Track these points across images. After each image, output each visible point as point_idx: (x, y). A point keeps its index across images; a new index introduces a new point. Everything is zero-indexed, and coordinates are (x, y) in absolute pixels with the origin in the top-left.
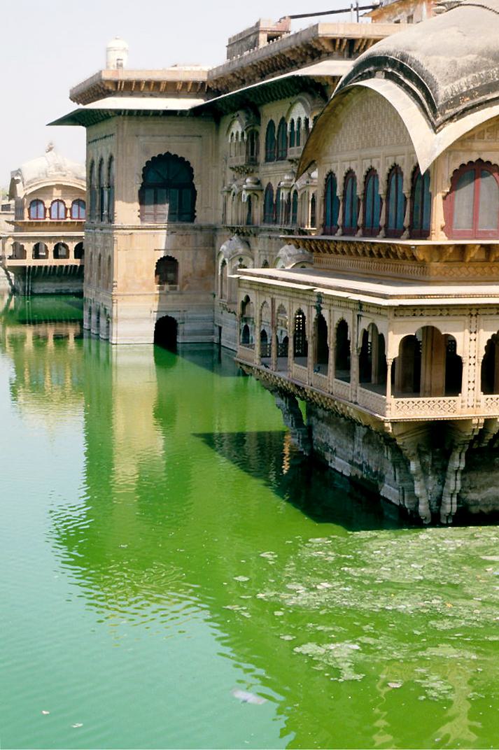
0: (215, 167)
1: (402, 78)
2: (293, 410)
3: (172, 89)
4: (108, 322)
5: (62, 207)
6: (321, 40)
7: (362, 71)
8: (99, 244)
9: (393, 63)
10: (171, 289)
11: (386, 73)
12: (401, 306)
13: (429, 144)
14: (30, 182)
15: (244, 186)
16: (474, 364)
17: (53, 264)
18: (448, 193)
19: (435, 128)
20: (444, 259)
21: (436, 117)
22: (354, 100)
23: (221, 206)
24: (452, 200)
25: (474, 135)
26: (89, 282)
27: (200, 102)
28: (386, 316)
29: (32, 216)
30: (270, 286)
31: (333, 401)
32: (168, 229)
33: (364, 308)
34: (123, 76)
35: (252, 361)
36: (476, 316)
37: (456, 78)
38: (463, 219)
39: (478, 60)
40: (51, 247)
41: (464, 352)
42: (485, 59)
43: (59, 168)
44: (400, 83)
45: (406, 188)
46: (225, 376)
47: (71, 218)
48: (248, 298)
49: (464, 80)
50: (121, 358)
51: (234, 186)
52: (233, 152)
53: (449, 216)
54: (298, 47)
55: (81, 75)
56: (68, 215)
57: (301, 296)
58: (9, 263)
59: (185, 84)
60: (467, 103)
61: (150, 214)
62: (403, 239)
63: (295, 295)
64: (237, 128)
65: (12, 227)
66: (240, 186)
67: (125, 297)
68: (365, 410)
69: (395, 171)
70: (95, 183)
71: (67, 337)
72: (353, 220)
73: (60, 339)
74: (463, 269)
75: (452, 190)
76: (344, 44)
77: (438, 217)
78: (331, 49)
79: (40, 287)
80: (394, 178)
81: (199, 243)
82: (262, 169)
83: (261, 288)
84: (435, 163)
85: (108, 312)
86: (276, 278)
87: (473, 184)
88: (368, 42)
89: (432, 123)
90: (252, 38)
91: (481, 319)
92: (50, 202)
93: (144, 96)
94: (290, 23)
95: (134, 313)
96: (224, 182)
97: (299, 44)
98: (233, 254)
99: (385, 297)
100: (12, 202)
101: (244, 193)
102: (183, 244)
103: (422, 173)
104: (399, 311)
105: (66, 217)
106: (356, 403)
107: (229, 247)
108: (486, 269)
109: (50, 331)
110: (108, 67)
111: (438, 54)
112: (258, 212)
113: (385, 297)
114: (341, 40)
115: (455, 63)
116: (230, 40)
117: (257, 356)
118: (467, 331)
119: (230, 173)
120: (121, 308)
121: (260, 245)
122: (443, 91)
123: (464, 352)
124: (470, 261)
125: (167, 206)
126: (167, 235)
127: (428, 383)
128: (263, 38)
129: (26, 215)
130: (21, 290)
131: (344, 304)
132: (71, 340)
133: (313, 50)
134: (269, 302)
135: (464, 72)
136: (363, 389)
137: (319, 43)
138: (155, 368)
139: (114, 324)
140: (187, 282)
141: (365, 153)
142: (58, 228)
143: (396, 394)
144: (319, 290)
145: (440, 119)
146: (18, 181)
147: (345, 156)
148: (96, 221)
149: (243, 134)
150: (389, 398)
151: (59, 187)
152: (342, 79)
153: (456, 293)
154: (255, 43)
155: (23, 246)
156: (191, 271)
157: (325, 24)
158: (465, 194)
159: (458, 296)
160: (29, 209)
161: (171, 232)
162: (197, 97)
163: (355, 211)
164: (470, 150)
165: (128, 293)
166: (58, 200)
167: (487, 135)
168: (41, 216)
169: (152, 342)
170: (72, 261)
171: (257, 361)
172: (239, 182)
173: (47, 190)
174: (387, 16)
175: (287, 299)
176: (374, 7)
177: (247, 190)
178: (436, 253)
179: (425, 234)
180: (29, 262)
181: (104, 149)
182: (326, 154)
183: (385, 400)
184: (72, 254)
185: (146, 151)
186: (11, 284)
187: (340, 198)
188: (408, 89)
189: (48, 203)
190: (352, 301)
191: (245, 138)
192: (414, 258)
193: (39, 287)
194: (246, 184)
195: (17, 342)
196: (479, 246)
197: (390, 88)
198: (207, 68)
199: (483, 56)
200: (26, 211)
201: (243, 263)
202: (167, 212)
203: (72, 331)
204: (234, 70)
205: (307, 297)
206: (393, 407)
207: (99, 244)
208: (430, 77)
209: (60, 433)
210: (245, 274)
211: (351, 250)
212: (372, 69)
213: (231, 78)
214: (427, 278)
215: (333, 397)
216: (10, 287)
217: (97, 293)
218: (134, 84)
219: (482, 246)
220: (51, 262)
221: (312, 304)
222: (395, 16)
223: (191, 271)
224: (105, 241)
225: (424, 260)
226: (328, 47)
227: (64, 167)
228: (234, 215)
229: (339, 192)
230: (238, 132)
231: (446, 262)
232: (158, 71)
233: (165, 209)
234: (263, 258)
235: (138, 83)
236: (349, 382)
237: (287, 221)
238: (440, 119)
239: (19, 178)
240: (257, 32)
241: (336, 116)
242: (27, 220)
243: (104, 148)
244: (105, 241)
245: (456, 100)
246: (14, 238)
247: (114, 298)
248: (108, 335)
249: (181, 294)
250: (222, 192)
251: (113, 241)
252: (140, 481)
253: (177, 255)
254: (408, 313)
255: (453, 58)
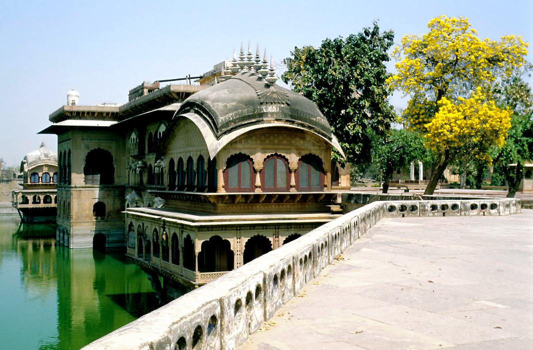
0: (124, 156)
1: (202, 113)
2: (156, 282)
3: (101, 116)
4: (68, 237)
5: (48, 176)
6: (172, 93)
7: (185, 108)
8: (64, 195)
9: (198, 106)
10: (102, 219)
11: (195, 110)
12: (201, 226)
13: (214, 144)
14: (31, 163)
15: (138, 165)
16: (240, 255)
17: (43, 206)
18: (225, 169)
19: (218, 138)
20: (224, 202)
21: (218, 132)
22: (181, 123)
23: (127, 176)
24: (227, 173)
25: (237, 141)
26: (59, 216)
27: (116, 122)
28: (194, 231)
29: (32, 181)
30: (142, 217)
31: (171, 275)
32: (100, 188)
33: (185, 227)
34: (75, 109)
35: (134, 255)
36: (239, 230)
37: (227, 114)
38: (234, 183)
39: (237, 105)
40: (42, 197)
41: (234, 248)
42: (241, 105)
43: (46, 156)
44: (201, 115)
45: (206, 167)
46: (127, 264)
47: (53, 182)
48: (131, 223)
49: (231, 114)
50: (74, 256)
51: (133, 165)
52: (132, 148)
53: (226, 180)
54: (161, 96)
55: (54, 108)
56: (52, 180)
57: (156, 222)
58: (19, 206)
59: (108, 114)
60: (233, 125)
61: (90, 180)
62: (205, 193)
63: (153, 221)
64: (134, 136)
65: (22, 187)
66: (136, 165)
67: (77, 224)
68: (186, 279)
69: (201, 158)
70: (62, 164)
71: (51, 245)
72: (183, 182)
73: (47, 247)
74: (234, 207)
75: (227, 167)
76: (184, 95)
77: (221, 182)
78: (177, 98)
79: (37, 219)
80: (200, 162)
81: (116, 195)
82: (147, 157)
83: (137, 218)
84: (218, 154)
85: (68, 232)
86: (144, 213)
87: (237, 165)
88: (188, 94)
89: (216, 135)
90: (140, 91)
91: (242, 232)
92: (42, 173)
93: (86, 119)
94: (159, 84)
95: (82, 233)
96: (128, 163)
97: (162, 95)
98: (133, 200)
99: (193, 221)
100: (22, 174)
101: (137, 169)
102: (108, 195)
103: (211, 159)
104: (201, 228)
105: (50, 182)
106: (182, 276)
107: (131, 197)
108: (246, 207)
109: (42, 242)
110: (68, 104)
111: (218, 101)
112: (145, 179)
113: (193, 221)
114: (183, 93)
115: (226, 106)
116: (130, 92)
117: (137, 253)
118: (235, 237)
119: (131, 159)
120: (75, 229)
121: (146, 196)
122: (221, 119)
123: (234, 248)
124: (238, 203)
125: (99, 175)
126: (99, 191)
127: (219, 265)
128: (146, 91)
129: (29, 181)
130: (26, 220)
131: (175, 225)
132: (53, 247)
133: (168, 97)
134: (141, 225)
135: (230, 111)
136: (185, 269)
137: (172, 95)
138: (94, 262)
139: (72, 238)
140: (110, 215)
141: (187, 149)
142: (46, 187)
143: (201, 270)
144: (164, 218)
145: (219, 133)
146: (25, 163)
147: (179, 151)
148: (62, 184)
149: (136, 139)
150: (197, 273)
151: (47, 166)
152: (176, 113)
153: (229, 219)
154: (142, 93)
155: (27, 197)
156: (112, 209)
157: (173, 85)
158: (234, 170)
159: (230, 220)
160: (30, 178)
161: (101, 189)
162: (114, 120)
163: (204, 178)
164: (236, 149)
165: (78, 221)
166: (46, 173)
167: (243, 141)
168: (37, 181)
169: (92, 246)
170: (53, 205)
171: (136, 256)
172: (135, 163)
173: (41, 167)
174: (207, 82)
175: (150, 223)
176: (201, 77)
177: (139, 167)
178: (220, 199)
179: (215, 190)
180: (30, 205)
181: (66, 146)
182: (169, 150)
183: (195, 274)
184: (53, 201)
185: (87, 147)
186: (21, 217)
187: (177, 172)
188: (205, 119)
189: (40, 174)
190: (179, 224)
191: (138, 141)
192: (210, 202)
193: (36, 219)
194: (138, 164)
195: (24, 249)
196: (240, 196)
197: (196, 118)
198: (118, 106)
199: (240, 103)
200: (29, 178)
201: (138, 205)
202: (99, 179)
203: (53, 242)
204: (131, 107)
205: (159, 222)
206: (199, 277)
207: (64, 195)
208: (215, 113)
209: (47, 296)
210: (130, 211)
211: (181, 198)
212: (188, 108)
213: (130, 111)
214: (216, 212)
215: (172, 273)
216: (20, 219)
217: (63, 221)
218: (110, 114)
219: (242, 195)
220: (42, 205)
221: (161, 226)
222: (211, 82)
223: (112, 209)
224: (67, 194)
225: (214, 203)
226: (176, 96)
227: (49, 155)
228: (133, 180)
229: (176, 169)
230: (134, 138)
231: (225, 203)
232: (94, 106)
233: (98, 177)
234: (148, 202)
235: (83, 113)
236: (178, 265)
237: (159, 184)
238: (219, 133)
239: (25, 161)
240: (143, 88)
241: (173, 131)
242: (29, 183)
243: (66, 146)
244: (67, 194)
245: (227, 124)
246: (22, 193)
247: (72, 224)
248: (68, 244)
249: (107, 221)
250: (127, 171)
251: (71, 194)
252: (85, 322)
253: (105, 201)
254: (205, 229)
255: (225, 104)
